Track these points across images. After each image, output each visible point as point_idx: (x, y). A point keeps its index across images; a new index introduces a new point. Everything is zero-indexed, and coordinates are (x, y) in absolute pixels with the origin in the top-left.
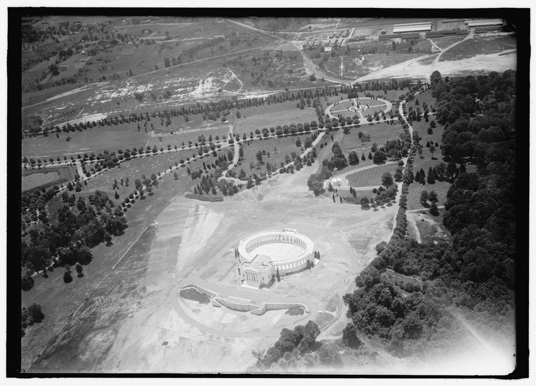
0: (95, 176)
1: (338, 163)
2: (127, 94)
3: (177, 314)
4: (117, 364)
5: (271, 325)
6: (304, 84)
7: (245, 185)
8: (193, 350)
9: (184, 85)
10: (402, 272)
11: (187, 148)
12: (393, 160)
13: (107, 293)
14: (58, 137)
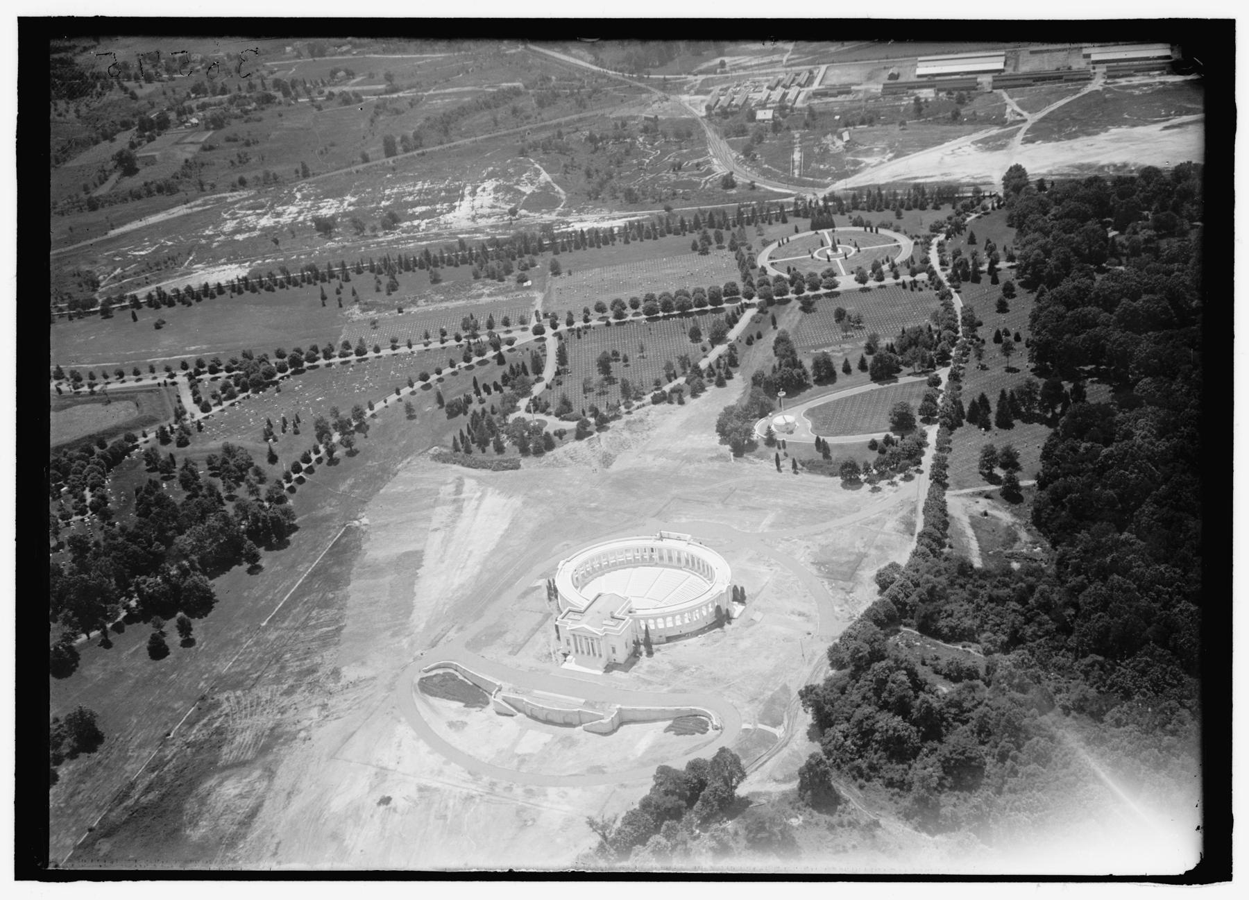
0: (222, 410)
1: (788, 381)
2: (295, 218)
3: (412, 733)
4: (272, 848)
5: (632, 758)
6: (708, 197)
7: (571, 431)
8: (450, 815)
9: (429, 198)
10: (936, 634)
11: (435, 345)
12: (915, 374)
13: (249, 682)
14: (135, 319)
